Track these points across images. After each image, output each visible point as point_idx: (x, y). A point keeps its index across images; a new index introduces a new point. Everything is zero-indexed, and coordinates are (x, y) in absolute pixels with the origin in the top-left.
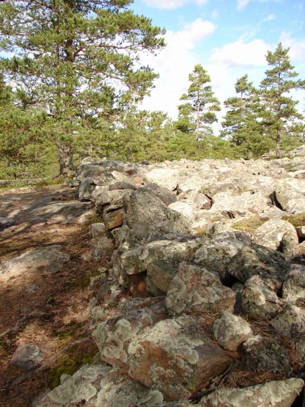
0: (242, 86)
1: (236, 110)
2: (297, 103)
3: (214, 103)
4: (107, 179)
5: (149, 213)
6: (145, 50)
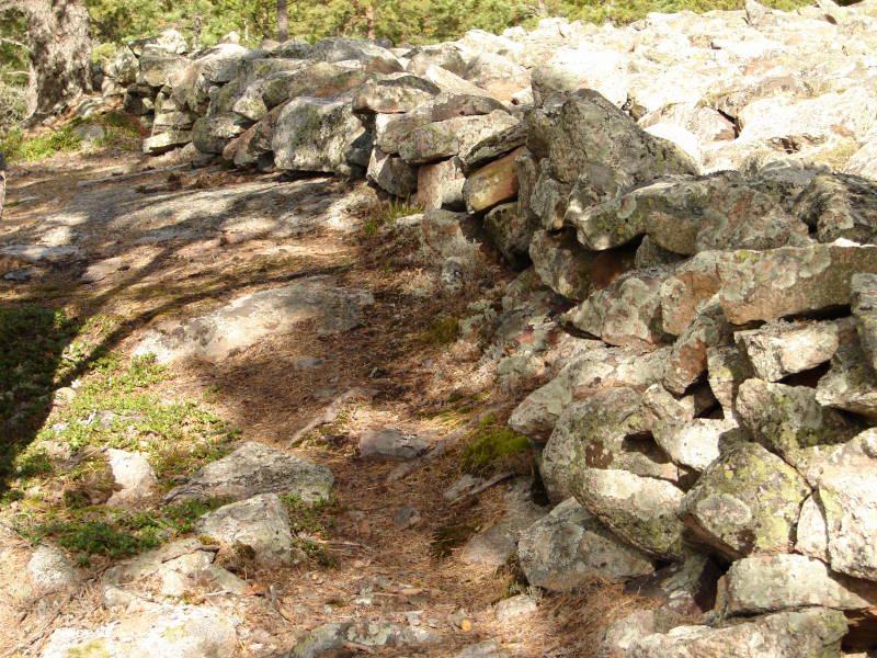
4: (405, 93)
5: (609, 140)
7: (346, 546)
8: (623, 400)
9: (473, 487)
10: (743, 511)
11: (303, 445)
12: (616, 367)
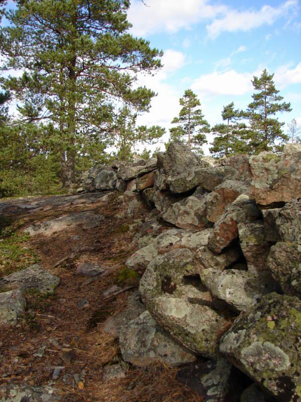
0: (228, 113)
1: (223, 136)
2: (283, 124)
3: (204, 125)
6: (143, 71)
7: (48, 318)
8: (183, 255)
9: (116, 291)
10: (282, 358)
11: (59, 267)
12: (181, 238)
